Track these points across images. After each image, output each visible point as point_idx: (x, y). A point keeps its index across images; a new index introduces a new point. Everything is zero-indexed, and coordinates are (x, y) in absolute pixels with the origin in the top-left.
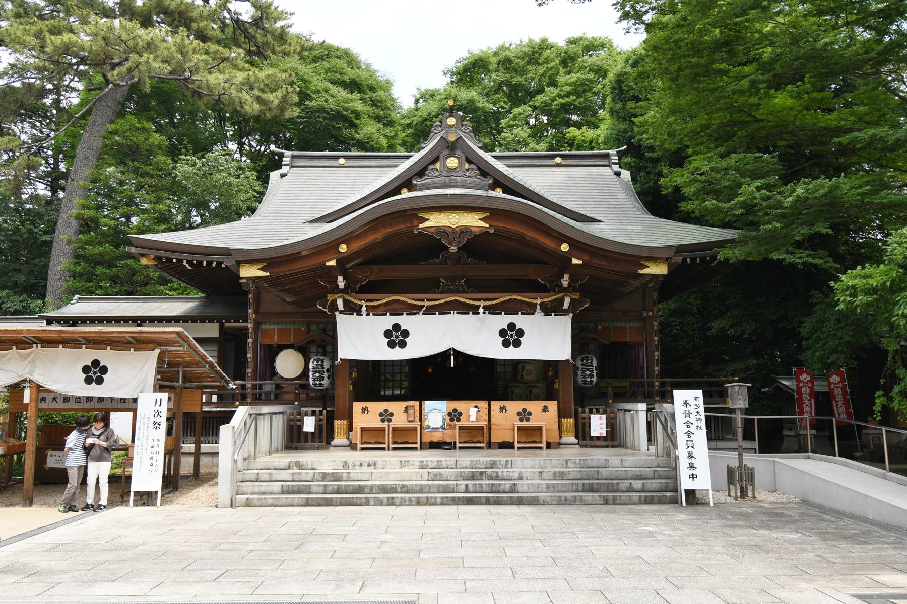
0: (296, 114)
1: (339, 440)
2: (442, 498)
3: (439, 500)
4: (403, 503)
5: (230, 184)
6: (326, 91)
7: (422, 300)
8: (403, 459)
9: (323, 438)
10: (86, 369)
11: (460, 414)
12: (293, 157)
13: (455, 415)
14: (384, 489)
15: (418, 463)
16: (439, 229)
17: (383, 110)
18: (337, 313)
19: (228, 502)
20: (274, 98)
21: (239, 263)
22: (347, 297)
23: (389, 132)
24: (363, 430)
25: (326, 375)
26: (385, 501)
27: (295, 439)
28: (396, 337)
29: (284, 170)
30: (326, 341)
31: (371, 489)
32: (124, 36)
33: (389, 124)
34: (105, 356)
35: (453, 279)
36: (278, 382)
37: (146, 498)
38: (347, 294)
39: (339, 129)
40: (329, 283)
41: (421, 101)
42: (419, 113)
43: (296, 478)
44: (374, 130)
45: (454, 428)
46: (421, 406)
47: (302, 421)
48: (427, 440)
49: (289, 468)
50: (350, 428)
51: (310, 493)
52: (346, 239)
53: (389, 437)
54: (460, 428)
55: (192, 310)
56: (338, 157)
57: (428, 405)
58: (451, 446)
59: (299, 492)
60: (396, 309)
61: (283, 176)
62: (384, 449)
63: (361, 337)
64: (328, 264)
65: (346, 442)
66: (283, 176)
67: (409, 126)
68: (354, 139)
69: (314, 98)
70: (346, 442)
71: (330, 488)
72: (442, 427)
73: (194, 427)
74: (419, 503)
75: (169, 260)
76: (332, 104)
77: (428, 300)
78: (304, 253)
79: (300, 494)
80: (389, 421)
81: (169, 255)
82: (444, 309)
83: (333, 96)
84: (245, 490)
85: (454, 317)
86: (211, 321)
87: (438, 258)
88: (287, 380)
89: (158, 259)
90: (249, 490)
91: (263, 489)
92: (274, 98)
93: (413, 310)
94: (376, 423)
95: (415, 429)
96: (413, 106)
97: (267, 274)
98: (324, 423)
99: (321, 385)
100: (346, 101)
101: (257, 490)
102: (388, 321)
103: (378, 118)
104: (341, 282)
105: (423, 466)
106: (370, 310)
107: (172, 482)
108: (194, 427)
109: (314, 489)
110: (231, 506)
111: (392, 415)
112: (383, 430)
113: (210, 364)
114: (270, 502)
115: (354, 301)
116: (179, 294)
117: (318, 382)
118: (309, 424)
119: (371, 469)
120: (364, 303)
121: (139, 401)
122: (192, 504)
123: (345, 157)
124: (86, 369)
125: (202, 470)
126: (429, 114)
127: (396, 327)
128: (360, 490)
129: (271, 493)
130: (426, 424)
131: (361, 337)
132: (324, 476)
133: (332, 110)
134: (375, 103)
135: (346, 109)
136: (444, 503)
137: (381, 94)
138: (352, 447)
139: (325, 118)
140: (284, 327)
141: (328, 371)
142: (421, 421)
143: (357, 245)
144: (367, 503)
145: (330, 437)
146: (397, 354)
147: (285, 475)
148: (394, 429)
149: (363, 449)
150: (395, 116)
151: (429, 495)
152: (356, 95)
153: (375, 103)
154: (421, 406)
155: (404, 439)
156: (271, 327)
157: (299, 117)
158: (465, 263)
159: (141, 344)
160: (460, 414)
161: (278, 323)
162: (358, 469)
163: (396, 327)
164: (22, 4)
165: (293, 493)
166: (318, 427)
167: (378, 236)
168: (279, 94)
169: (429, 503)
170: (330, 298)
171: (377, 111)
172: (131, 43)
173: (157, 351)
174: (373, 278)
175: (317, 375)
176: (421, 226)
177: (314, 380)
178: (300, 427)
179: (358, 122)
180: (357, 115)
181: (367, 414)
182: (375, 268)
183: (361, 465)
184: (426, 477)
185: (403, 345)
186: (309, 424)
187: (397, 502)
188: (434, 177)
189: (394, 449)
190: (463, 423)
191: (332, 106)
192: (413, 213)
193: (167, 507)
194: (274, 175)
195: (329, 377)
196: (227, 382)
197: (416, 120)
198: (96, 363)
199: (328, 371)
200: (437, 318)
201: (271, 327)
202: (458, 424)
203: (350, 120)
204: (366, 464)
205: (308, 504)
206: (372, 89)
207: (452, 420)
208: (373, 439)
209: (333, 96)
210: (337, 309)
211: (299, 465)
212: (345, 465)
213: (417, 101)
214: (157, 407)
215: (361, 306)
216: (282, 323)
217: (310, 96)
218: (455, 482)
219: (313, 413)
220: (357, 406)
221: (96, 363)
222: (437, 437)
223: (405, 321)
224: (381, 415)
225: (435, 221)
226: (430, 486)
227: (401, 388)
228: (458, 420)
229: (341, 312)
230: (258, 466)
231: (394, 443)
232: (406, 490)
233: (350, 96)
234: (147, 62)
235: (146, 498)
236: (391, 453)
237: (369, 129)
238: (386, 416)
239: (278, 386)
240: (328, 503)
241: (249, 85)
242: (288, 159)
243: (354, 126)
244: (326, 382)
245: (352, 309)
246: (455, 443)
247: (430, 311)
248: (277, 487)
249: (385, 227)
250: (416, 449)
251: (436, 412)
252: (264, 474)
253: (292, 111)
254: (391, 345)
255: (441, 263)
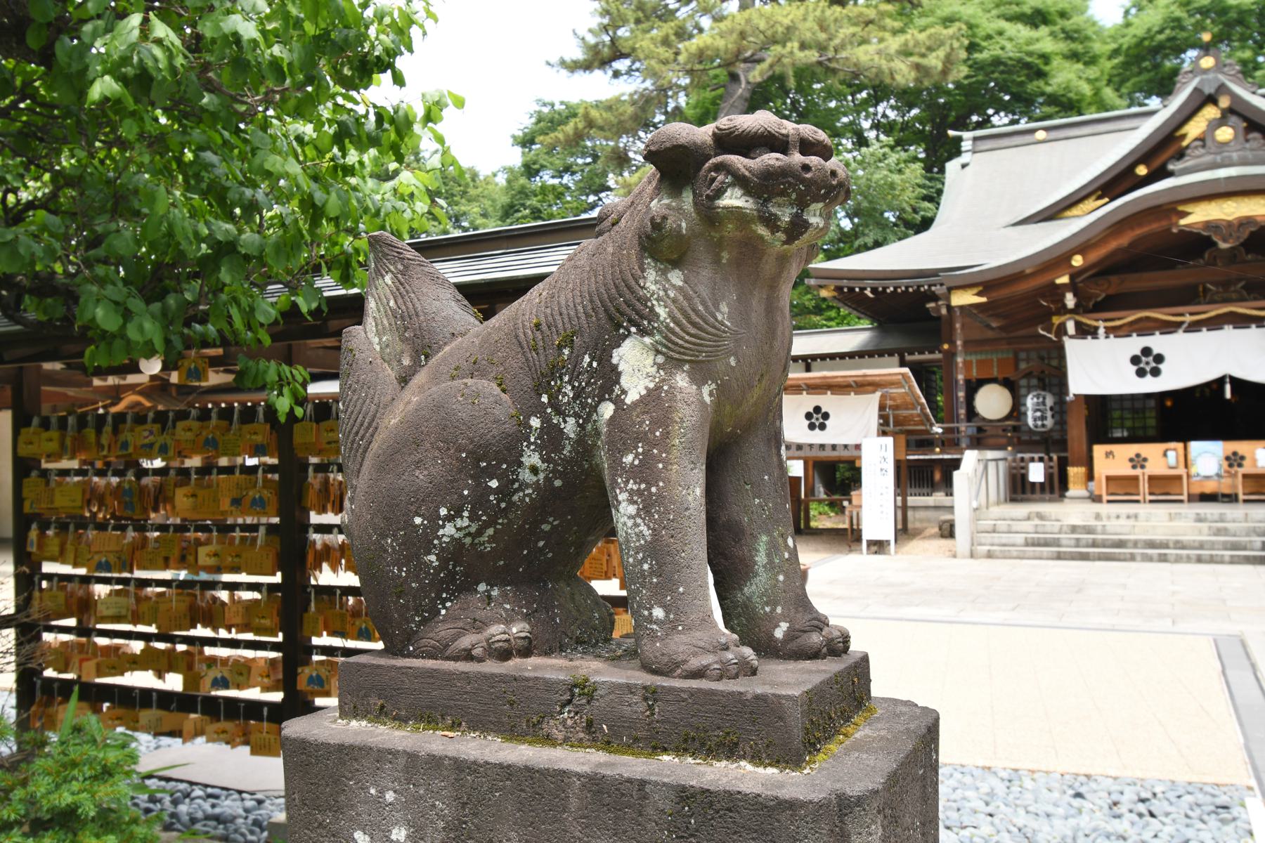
0: (962, 75)
1: (1075, 490)
2: (1232, 556)
3: (1227, 559)
4: (1178, 559)
5: (892, 186)
6: (1000, 33)
7: (1182, 315)
8: (1173, 511)
9: (1056, 486)
10: (808, 416)
11: (1242, 458)
12: (975, 139)
13: (1234, 460)
14: (1151, 544)
15: (1194, 516)
16: (1208, 225)
17: (1082, 43)
18: (1065, 339)
19: (967, 553)
20: (934, 61)
21: (950, 289)
22: (1079, 318)
23: (1092, 72)
24: (1109, 479)
25: (1049, 414)
26: (1156, 557)
27: (1019, 488)
28: (1147, 363)
29: (965, 158)
30: (1052, 375)
31: (1135, 544)
32: (762, 25)
33: (1092, 61)
34: (827, 401)
35: (1226, 284)
36: (980, 424)
37: (878, 546)
38: (1077, 313)
39: (1022, 84)
40: (1053, 302)
41: (1133, 11)
42: (1132, 31)
43: (1040, 529)
44: (1072, 76)
45: (1235, 475)
46: (1185, 448)
47: (1026, 468)
48: (1197, 490)
49: (1028, 519)
50: (1090, 476)
51: (1059, 546)
52: (1082, 250)
53: (1144, 486)
54: (1245, 476)
55: (867, 344)
56: (1033, 131)
57: (1195, 446)
58: (1231, 498)
59: (1046, 544)
60: (1144, 328)
61: (964, 166)
62: (1137, 501)
63: (1099, 366)
64: (1059, 281)
65: (1084, 493)
66: (964, 166)
67: (1116, 52)
68: (1043, 94)
69: (984, 48)
70: (1084, 493)
71: (1083, 542)
72: (1218, 475)
73: (922, 474)
74: (1199, 560)
75: (851, 289)
76: (1011, 52)
77: (1192, 314)
78: (1028, 271)
79: (1045, 546)
80: (1143, 467)
81: (852, 284)
82: (1215, 324)
83: (1010, 39)
84: (983, 541)
85: (1228, 332)
86: (891, 354)
87: (1202, 257)
88: (991, 421)
89: (839, 289)
90: (989, 541)
91: (1004, 541)
92: (934, 61)
93: (1168, 328)
94: (1126, 470)
95: (1179, 478)
96: (1119, 20)
97: (984, 300)
98: (1055, 471)
99: (1043, 426)
100: (1030, 42)
101: (996, 541)
102: (1135, 344)
103: (1074, 56)
104: (1070, 300)
105: (1200, 519)
106: (1109, 331)
107: (904, 531)
108: (922, 474)
109: (1064, 542)
110: (972, 556)
111: (1145, 460)
112: (1136, 478)
113: (922, 405)
114: (1015, 554)
115: (1089, 322)
116: (838, 324)
117: (1039, 423)
118: (1036, 473)
119: (1131, 522)
120: (1101, 324)
121: (863, 448)
122: (924, 556)
123: (1046, 129)
124: (808, 416)
125: (910, 526)
126: (1149, 30)
127: (1146, 351)
128: (1121, 544)
129: (1013, 545)
130: (1193, 471)
131: (1099, 366)
132: (1074, 529)
133: (1010, 59)
134: (1069, 36)
135: (1030, 54)
136: (1234, 561)
137: (1075, 21)
138: (1096, 499)
139: (1002, 72)
140: (983, 357)
141: (1051, 409)
142: (1186, 466)
143: (1095, 256)
144: (1132, 558)
145: (1064, 485)
146: (1150, 385)
147: (1027, 526)
148: (1151, 478)
149: (1109, 501)
150: (1097, 47)
151: (1214, 552)
152: (1044, 30)
153: (1069, 36)
154: (1185, 448)
155: (1165, 488)
156: (989, 357)
157: (967, 77)
158: (1245, 262)
159: (862, 387)
160: (1242, 458)
161: (976, 353)
162: (1114, 522)
163: (1146, 351)
164: (640, 7)
165: (1039, 545)
166: (1049, 476)
167: (1124, 240)
168: (941, 53)
169: (1212, 560)
170: (1056, 320)
171: (1074, 46)
172: (769, 33)
173: (878, 394)
174: (1112, 291)
175: (1038, 414)
176: (1183, 222)
177: (1035, 420)
178: (1024, 477)
179: (1047, 68)
180: (1046, 58)
181: (1112, 460)
182: (1114, 279)
183: (1118, 517)
184: (1206, 531)
185: (1156, 372)
186: (1036, 473)
187: (1172, 559)
188: (1198, 157)
189: (1151, 501)
190: (1247, 468)
191: (1011, 54)
192: (1170, 208)
193: (899, 556)
194: (952, 166)
195: (1053, 416)
196: (932, 425)
197: (1126, 42)
198: (817, 409)
199: (1051, 409)
200: (1205, 335)
201: (989, 357)
202: (1241, 471)
203: (1035, 69)
204: (1124, 516)
205: (1059, 557)
206: (1063, 14)
207: (1231, 466)
208: (1123, 488)
209: (1010, 39)
210: (1066, 333)
211: (1041, 516)
212: (1098, 517)
213: (1127, 12)
214: (883, 453)
215: (1097, 328)
216: (981, 352)
217: (978, 45)
218: (1247, 539)
219: (1041, 460)
220: (1099, 450)
221: (817, 409)
222: (1209, 488)
223: (1157, 342)
224: (1131, 460)
225: (1199, 215)
226: (1213, 543)
227: (1122, 427)
228: (1240, 465)
229: (1071, 337)
230: (992, 516)
231: (1151, 494)
232: (1180, 545)
233: (1034, 34)
234: (792, 53)
235: (878, 546)
236: (1148, 505)
237: (1065, 76)
238: (1138, 462)
239: (980, 429)
240: (1084, 557)
241: (905, 52)
242: (970, 142)
243: (1041, 74)
244: (1049, 422)
245: (1085, 332)
246: (1236, 495)
247: (1194, 327)
248: (1020, 539)
249: (1132, 229)
250: (1181, 501)
251: (1207, 457)
252: (1002, 525)
253: (959, 71)
254: (1141, 373)
255: (1207, 264)
